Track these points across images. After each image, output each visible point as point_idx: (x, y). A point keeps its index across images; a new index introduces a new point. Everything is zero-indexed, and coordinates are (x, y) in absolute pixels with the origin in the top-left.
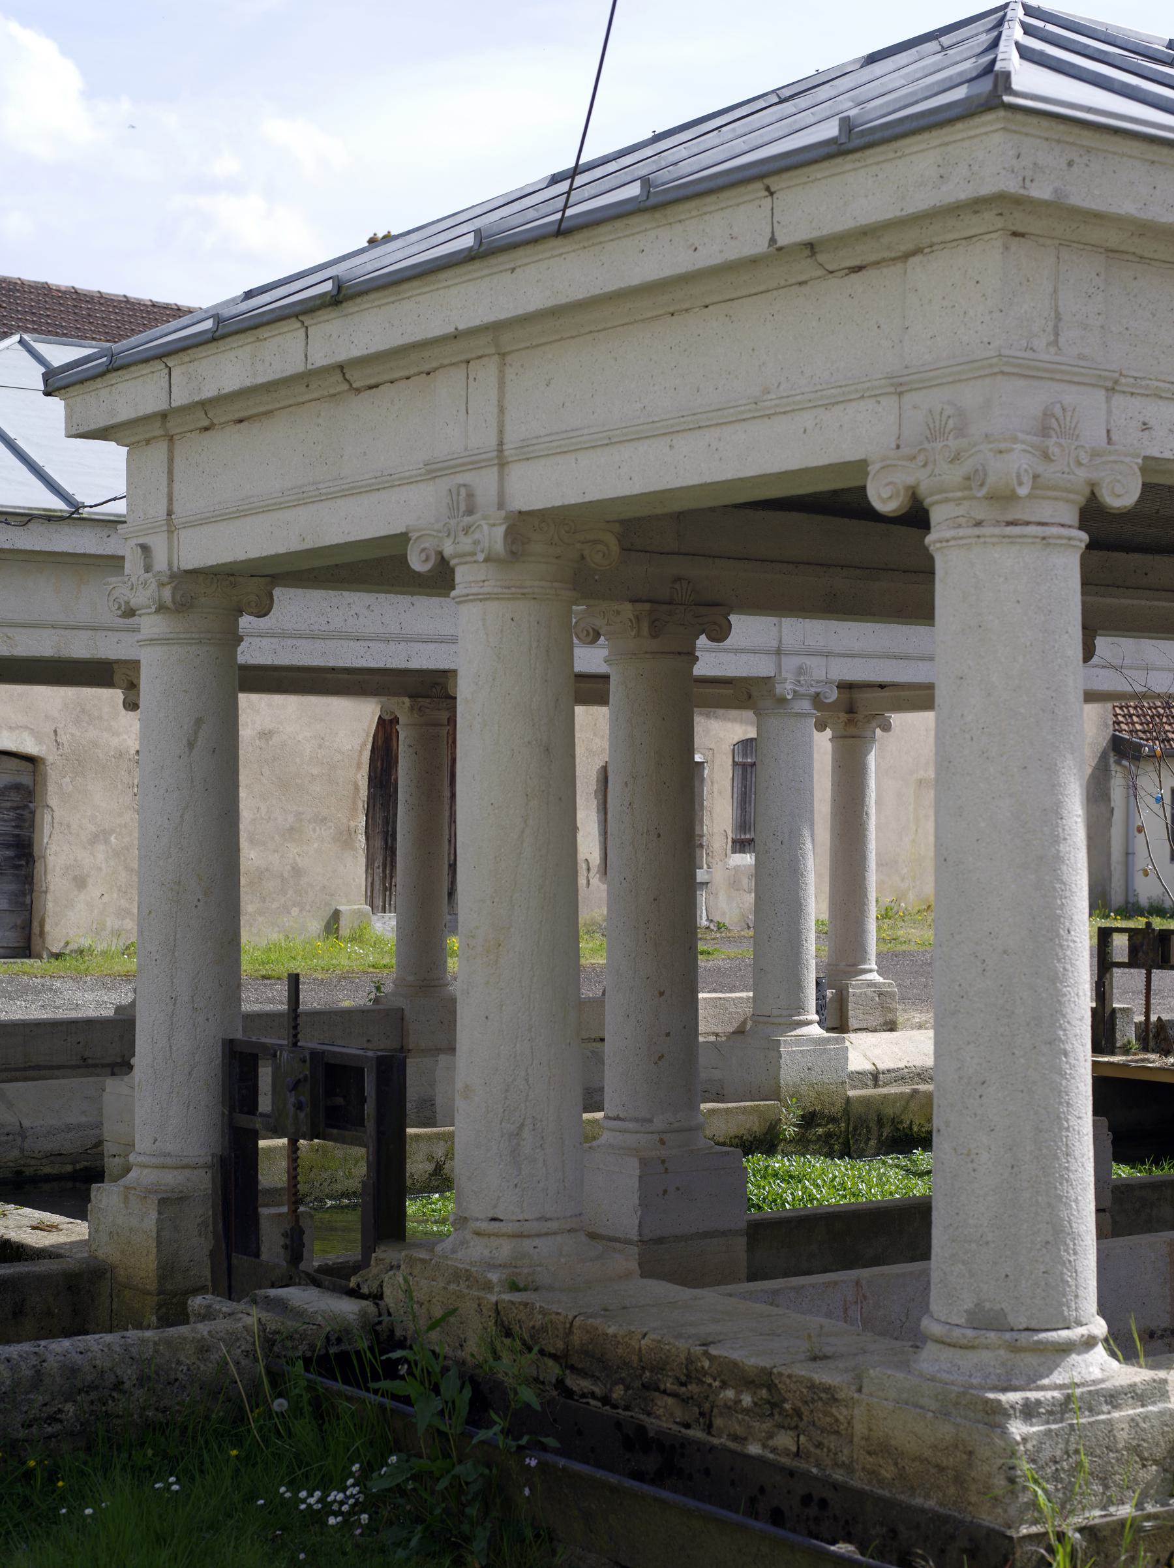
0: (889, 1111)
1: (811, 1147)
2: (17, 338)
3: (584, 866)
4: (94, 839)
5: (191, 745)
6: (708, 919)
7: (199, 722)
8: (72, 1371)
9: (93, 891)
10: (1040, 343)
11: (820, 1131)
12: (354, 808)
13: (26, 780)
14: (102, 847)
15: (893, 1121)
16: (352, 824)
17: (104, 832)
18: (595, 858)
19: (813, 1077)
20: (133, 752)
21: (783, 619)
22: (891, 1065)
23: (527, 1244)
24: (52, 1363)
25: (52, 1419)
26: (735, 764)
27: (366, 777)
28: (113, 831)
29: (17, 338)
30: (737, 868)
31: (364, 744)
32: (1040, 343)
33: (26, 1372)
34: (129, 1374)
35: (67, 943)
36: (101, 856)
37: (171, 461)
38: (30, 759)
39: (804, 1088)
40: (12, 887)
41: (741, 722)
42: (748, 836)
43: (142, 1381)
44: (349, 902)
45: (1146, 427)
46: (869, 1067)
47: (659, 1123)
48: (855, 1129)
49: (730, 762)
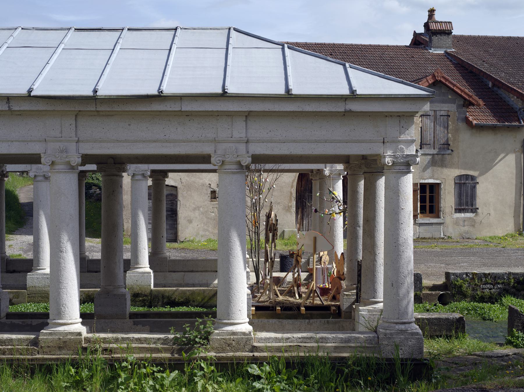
0: (167, 294)
4: (194, 209)
6: (444, 235)
9: (195, 224)
11: (141, 299)
12: (291, 199)
13: (174, 193)
15: (168, 297)
16: (290, 204)
17: (198, 207)
19: (138, 283)
20: (208, 184)
21: (33, 165)
26: (455, 183)
27: (295, 190)
28: (201, 207)
30: (457, 218)
31: (294, 180)
35: (185, 239)
38: (176, 187)
39: (135, 286)
40: (171, 222)
41: (459, 169)
42: (462, 207)
44: (289, 228)
48: (154, 299)
49: (453, 182)
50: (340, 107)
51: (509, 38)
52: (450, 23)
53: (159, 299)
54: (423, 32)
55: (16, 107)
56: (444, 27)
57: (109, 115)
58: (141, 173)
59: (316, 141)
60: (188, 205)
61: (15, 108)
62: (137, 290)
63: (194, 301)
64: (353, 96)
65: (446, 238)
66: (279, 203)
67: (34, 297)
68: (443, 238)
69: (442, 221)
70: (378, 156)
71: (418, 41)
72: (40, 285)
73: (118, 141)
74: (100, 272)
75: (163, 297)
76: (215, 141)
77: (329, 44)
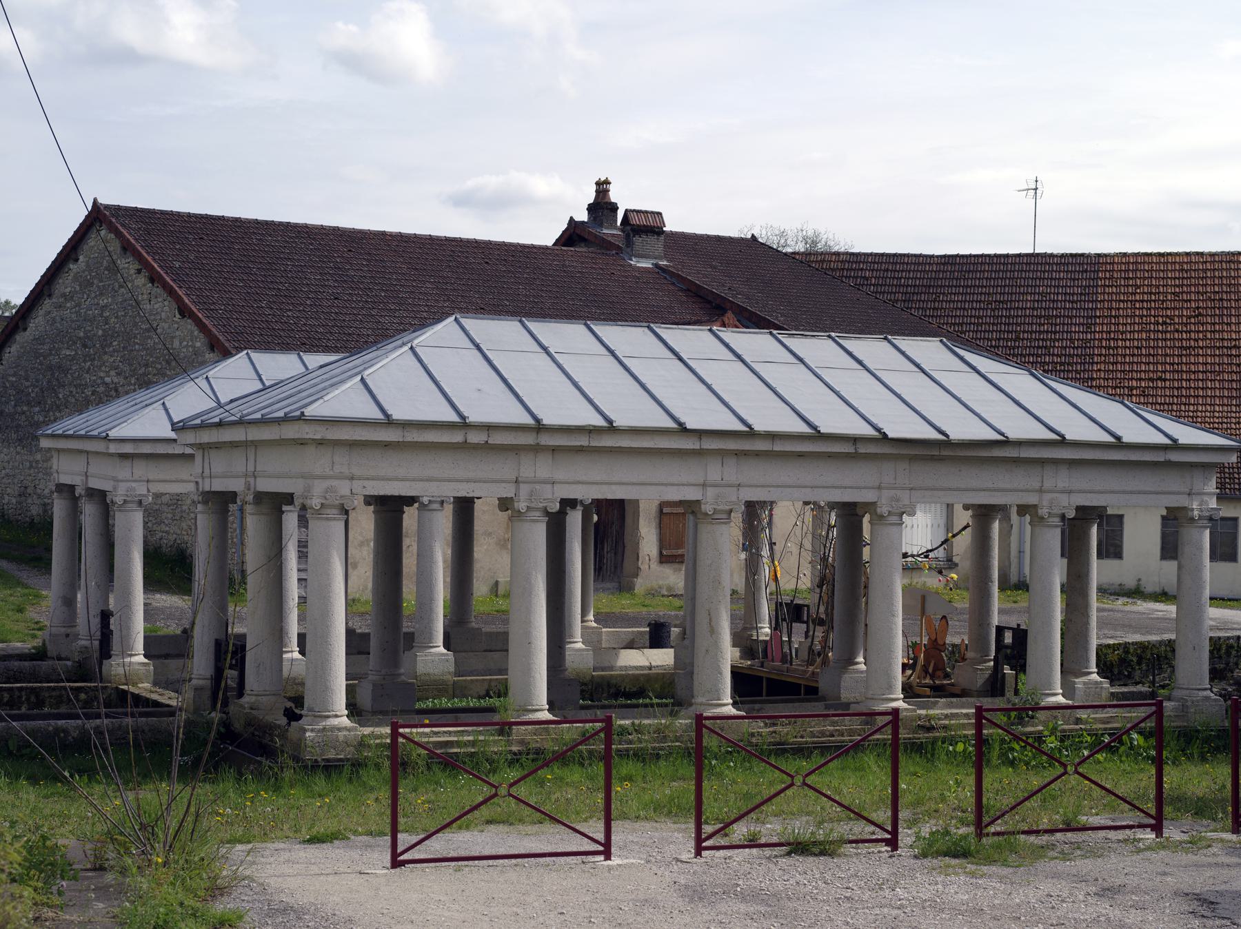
0: (614, 682)
22: (659, 663)
36: (365, 553)
46: (647, 664)
50: (1160, 457)
51: (719, 239)
52: (660, 214)
55: (862, 449)
56: (651, 222)
57: (941, 459)
58: (192, 478)
59: (1131, 492)
61: (862, 450)
64: (1175, 446)
66: (490, 534)
70: (1185, 508)
71: (573, 235)
72: (436, 671)
73: (950, 489)
75: (609, 685)
76: (1041, 491)
77: (281, 224)
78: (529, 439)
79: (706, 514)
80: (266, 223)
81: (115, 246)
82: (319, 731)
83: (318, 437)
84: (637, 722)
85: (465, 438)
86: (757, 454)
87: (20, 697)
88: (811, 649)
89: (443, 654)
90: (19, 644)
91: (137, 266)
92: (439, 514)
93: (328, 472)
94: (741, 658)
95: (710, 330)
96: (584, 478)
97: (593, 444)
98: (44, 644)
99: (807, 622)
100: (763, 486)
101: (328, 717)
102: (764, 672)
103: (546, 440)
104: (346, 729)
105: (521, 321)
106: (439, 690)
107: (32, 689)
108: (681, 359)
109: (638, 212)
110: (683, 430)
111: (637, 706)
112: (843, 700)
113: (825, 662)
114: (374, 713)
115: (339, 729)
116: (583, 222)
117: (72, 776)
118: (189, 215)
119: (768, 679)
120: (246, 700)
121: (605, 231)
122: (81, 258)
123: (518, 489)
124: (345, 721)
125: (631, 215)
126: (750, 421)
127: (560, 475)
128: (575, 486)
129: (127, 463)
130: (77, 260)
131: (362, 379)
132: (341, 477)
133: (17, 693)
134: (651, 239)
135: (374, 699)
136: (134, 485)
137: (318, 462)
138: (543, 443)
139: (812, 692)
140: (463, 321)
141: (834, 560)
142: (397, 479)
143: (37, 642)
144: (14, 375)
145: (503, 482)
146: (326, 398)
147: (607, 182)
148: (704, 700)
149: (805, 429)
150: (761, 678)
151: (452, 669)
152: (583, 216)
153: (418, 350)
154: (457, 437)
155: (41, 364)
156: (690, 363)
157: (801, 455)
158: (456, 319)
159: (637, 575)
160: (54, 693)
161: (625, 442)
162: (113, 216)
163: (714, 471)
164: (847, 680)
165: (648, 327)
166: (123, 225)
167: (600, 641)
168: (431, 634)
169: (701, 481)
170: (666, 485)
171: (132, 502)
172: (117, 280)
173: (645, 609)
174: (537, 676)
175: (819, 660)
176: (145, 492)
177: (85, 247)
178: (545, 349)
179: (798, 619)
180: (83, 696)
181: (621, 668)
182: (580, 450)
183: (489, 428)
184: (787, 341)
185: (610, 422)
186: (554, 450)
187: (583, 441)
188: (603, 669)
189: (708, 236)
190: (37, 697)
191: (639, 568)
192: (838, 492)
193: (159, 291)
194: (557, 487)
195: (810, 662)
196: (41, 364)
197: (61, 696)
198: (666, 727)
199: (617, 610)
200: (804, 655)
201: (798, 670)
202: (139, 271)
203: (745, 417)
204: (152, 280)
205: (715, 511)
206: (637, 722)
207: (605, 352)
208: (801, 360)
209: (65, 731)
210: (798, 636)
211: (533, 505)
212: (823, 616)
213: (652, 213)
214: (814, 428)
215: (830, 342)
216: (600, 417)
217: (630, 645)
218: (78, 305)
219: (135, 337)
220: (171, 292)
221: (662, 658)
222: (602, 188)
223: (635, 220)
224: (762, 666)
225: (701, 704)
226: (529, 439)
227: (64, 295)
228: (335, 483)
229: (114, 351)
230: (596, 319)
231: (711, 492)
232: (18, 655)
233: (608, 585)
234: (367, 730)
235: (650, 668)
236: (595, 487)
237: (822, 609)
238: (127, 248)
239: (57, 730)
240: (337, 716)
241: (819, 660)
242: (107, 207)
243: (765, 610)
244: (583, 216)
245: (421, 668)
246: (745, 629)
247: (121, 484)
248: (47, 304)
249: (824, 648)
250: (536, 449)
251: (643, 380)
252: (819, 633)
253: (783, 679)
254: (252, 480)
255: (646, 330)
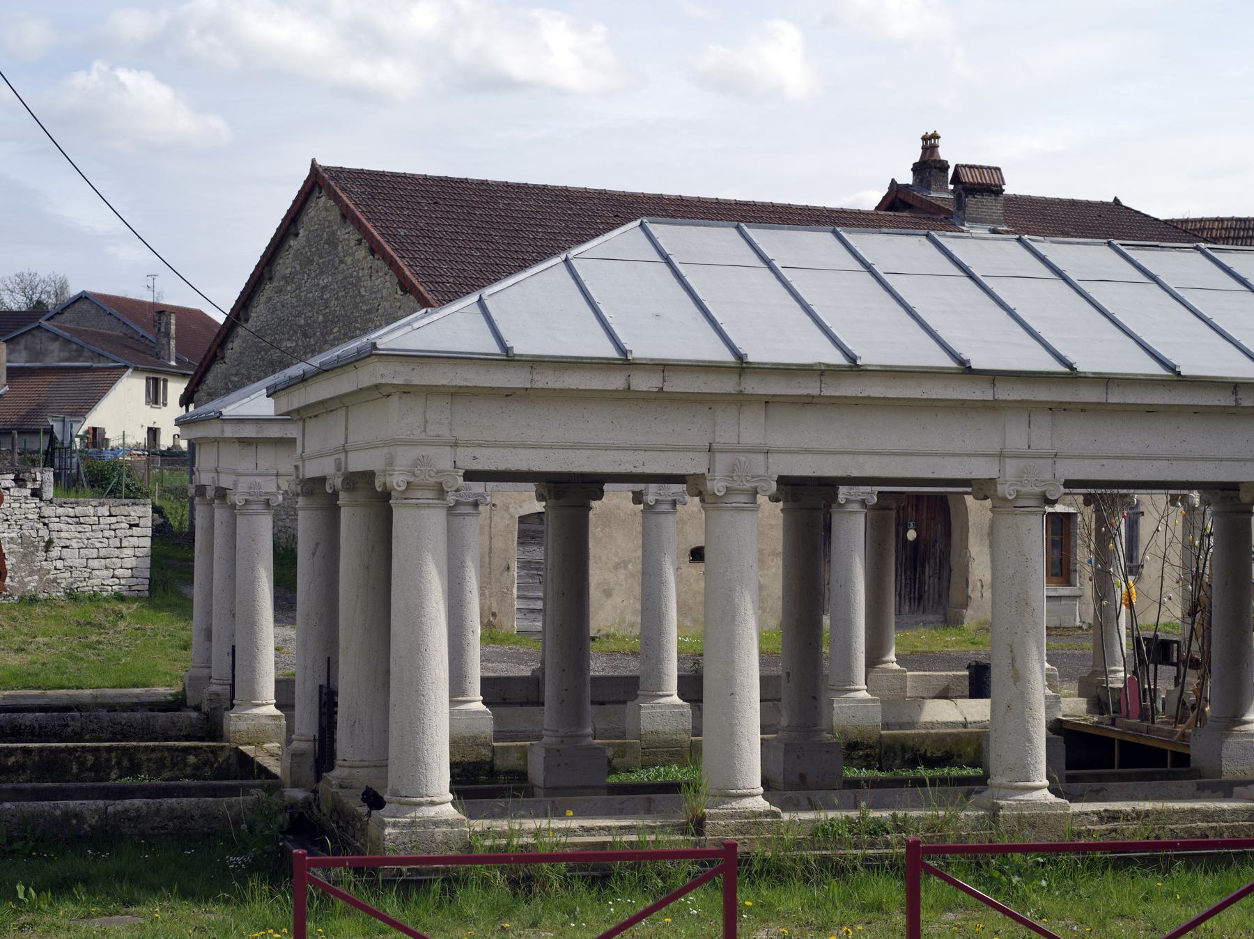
0: (910, 743)
1: (855, 762)
2: (638, 222)
3: (979, 584)
4: (617, 567)
5: (314, 554)
7: (317, 544)
8: (172, 810)
9: (617, 598)
10: (417, 432)
14: (622, 571)
17: (624, 562)
18: (987, 577)
22: (977, 718)
23: (355, 771)
24: (165, 806)
25: (163, 828)
29: (638, 222)
32: (417, 432)
33: (153, 808)
34: (196, 813)
36: (622, 577)
37: (304, 430)
39: (850, 728)
43: (202, 816)
45: (475, 458)
46: (961, 719)
47: (561, 732)
51: (1073, 204)
53: (895, 754)
54: (910, 182)
56: (987, 179)
60: (604, 558)
62: (854, 736)
63: (960, 756)
65: (1085, 627)
67: (655, 754)
68: (1080, 628)
69: (1078, 593)
72: (667, 729)
74: (543, 704)
75: (903, 748)
77: (535, 187)
78: (727, 385)
79: (1005, 499)
80: (518, 186)
81: (335, 214)
82: (404, 826)
83: (399, 381)
84: (900, 814)
85: (628, 384)
86: (1084, 409)
87: (109, 760)
88: (1182, 703)
89: (676, 706)
90: (161, 690)
91: (357, 236)
92: (670, 518)
93: (418, 434)
94: (1089, 711)
95: (1019, 240)
96: (815, 445)
97: (826, 392)
98: (184, 690)
99: (1176, 665)
100: (1093, 458)
101: (420, 804)
102: (1115, 732)
103: (753, 386)
104: (446, 822)
105: (738, 228)
106: (671, 754)
107: (125, 749)
108: (971, 276)
109: (971, 167)
110: (966, 370)
111: (920, 782)
112: (1226, 777)
113: (1201, 716)
114: (553, 791)
115: (437, 824)
116: (907, 186)
117: (26, 894)
118: (425, 178)
119: (1121, 742)
120: (337, 773)
121: (933, 195)
122: (301, 232)
123: (712, 462)
124: (448, 811)
125: (963, 172)
126: (1071, 358)
127: (777, 439)
128: (801, 457)
129: (250, 451)
130: (297, 235)
131: (480, 300)
132: (439, 442)
133: (105, 755)
134: (988, 200)
135: (547, 769)
136: (258, 480)
137: (398, 420)
138: (749, 390)
139: (1182, 760)
140: (651, 227)
141: (1210, 576)
142: (524, 446)
143: (177, 689)
144: (236, 375)
145: (689, 450)
146: (416, 325)
147: (935, 136)
148: (1004, 781)
149: (1156, 369)
150: (1113, 739)
151: (689, 726)
152: (906, 178)
153: (574, 262)
154: (615, 382)
155: (262, 359)
156: (986, 281)
157: (1151, 410)
158: (641, 225)
159: (966, 606)
160: (154, 756)
161: (876, 390)
162: (333, 178)
163: (1016, 435)
164: (1231, 745)
165: (927, 236)
166: (343, 189)
167: (904, 689)
168: (660, 678)
169: (997, 450)
170: (943, 455)
171: (256, 502)
172: (336, 255)
173: (974, 647)
174: (745, 744)
175: (1192, 715)
176: (274, 489)
177: (305, 219)
178: (768, 263)
179: (1166, 660)
180: (192, 759)
181: (933, 725)
182: (808, 402)
183: (664, 367)
184: (1133, 254)
185: (852, 358)
186: (768, 402)
187: (810, 388)
188: (901, 726)
189: (1061, 200)
190: (131, 760)
191: (968, 597)
192: (1210, 465)
193: (380, 263)
194: (772, 458)
195: (1179, 719)
196: (262, 359)
197: (162, 759)
198: (947, 822)
199: (936, 648)
200: (1172, 709)
201: (1163, 729)
202: (359, 242)
203: (1063, 352)
204: (372, 251)
205: (1019, 495)
206: (900, 814)
207: (856, 265)
208: (1154, 278)
209: (79, 816)
210: (1164, 681)
211: (735, 486)
212: (1198, 656)
213: (989, 168)
214: (1171, 368)
215: (1198, 255)
216: (838, 353)
217: (944, 695)
218: (298, 288)
219: (356, 321)
220: (391, 264)
221: (976, 710)
222: (930, 143)
223: (967, 177)
224: (1113, 724)
225: (1000, 787)
226: (727, 385)
227: (284, 277)
228: (430, 451)
229: (335, 339)
230: (845, 225)
231: (1011, 467)
232: (151, 703)
233: (931, 617)
234: (480, 825)
235: (965, 725)
236: (832, 458)
237: (1195, 646)
238: (346, 215)
239: (67, 815)
240: (433, 804)
241: (1192, 715)
242: (327, 169)
243: (1122, 642)
244: (906, 178)
245: (646, 725)
246: (1094, 673)
247: (242, 479)
248: (268, 289)
249: (1199, 699)
250: (740, 400)
251: (911, 303)
252: (1192, 678)
253: (1142, 742)
254: (342, 456)
255: (924, 239)
